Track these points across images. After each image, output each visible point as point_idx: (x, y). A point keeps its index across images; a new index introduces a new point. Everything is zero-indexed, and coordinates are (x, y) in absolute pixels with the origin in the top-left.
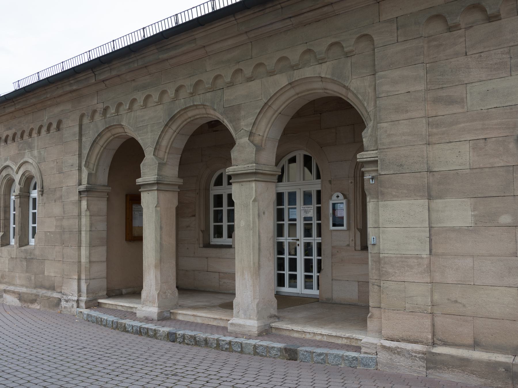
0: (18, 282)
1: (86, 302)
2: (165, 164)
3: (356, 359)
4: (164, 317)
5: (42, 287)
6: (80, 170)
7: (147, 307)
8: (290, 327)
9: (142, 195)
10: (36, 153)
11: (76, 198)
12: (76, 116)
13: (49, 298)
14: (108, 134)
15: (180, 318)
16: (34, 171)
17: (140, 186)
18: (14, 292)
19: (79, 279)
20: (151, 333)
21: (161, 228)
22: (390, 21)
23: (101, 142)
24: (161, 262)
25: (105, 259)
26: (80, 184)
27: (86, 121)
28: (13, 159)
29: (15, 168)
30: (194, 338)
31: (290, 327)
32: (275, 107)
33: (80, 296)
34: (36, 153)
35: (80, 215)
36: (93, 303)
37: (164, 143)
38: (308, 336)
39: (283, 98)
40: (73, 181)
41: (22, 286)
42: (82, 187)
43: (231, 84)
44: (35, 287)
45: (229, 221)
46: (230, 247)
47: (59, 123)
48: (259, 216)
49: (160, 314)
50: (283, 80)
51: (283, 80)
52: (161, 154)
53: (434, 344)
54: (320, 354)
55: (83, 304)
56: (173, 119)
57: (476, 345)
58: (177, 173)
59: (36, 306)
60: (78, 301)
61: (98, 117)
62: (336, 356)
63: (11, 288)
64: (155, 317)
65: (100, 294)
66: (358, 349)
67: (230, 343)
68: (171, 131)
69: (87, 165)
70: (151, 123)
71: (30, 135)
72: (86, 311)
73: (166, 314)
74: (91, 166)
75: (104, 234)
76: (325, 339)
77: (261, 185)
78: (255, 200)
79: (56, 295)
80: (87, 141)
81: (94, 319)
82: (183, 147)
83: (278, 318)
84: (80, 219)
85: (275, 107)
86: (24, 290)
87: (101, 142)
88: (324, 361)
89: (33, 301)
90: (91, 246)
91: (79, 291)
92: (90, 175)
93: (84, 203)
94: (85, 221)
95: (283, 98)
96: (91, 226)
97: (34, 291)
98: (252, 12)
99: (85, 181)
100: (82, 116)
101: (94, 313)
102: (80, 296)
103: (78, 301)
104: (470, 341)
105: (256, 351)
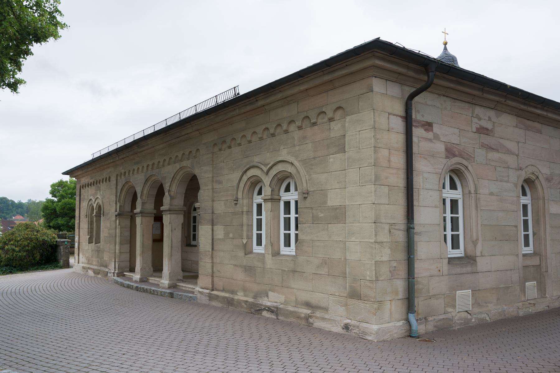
0: (94, 263)
1: (117, 274)
2: (146, 203)
3: (191, 297)
4: (142, 280)
5: (103, 266)
6: (116, 203)
7: (137, 276)
8: (184, 285)
9: (164, 216)
10: (101, 192)
11: (114, 218)
12: (115, 175)
13: (104, 271)
14: (127, 186)
15: (150, 281)
16: (101, 203)
17: (162, 211)
18: (92, 269)
19: (115, 262)
20: (159, 294)
21: (143, 235)
22: (204, 144)
23: (125, 189)
24: (143, 252)
25: (129, 251)
26: (116, 211)
27: (119, 178)
28: (94, 196)
29: (94, 200)
30: (143, 288)
31: (184, 285)
32: (178, 178)
33: (115, 270)
34: (101, 192)
35: (116, 228)
36: (121, 275)
37: (145, 192)
38: (187, 289)
39: (180, 174)
40: (113, 210)
41: (96, 265)
42: (117, 213)
43: (163, 166)
44: (100, 266)
45: (257, 230)
46: (195, 246)
47: (110, 178)
48: (172, 231)
49: (140, 279)
50: (177, 166)
51: (177, 166)
52: (144, 198)
53: (213, 290)
54: (180, 295)
55: (116, 275)
56: (147, 180)
57: (223, 290)
58: (153, 207)
59: (99, 276)
60: (114, 273)
61: (123, 177)
62: (185, 296)
63: (92, 267)
64: (138, 280)
65: (126, 270)
66: (193, 293)
67: (154, 290)
68: (147, 186)
69: (119, 201)
70: (170, 174)
71: (99, 183)
72: (116, 278)
73: (144, 279)
74: (121, 202)
75: (129, 238)
76: (190, 289)
77: (173, 216)
78: (169, 223)
79: (107, 270)
80: (119, 188)
81: (159, 294)
82: (155, 194)
83: (182, 281)
84: (116, 230)
85: (178, 178)
86: (96, 267)
87: (125, 189)
88: (181, 299)
89: (98, 273)
90: (121, 244)
91: (115, 268)
92: (120, 206)
93: (118, 221)
94: (118, 231)
95: (180, 174)
96: (121, 233)
97: (99, 268)
98: (91, 169)
99: (118, 210)
100: (117, 175)
101: (120, 280)
102: (115, 270)
103: (114, 273)
104: (222, 289)
105: (137, 289)
